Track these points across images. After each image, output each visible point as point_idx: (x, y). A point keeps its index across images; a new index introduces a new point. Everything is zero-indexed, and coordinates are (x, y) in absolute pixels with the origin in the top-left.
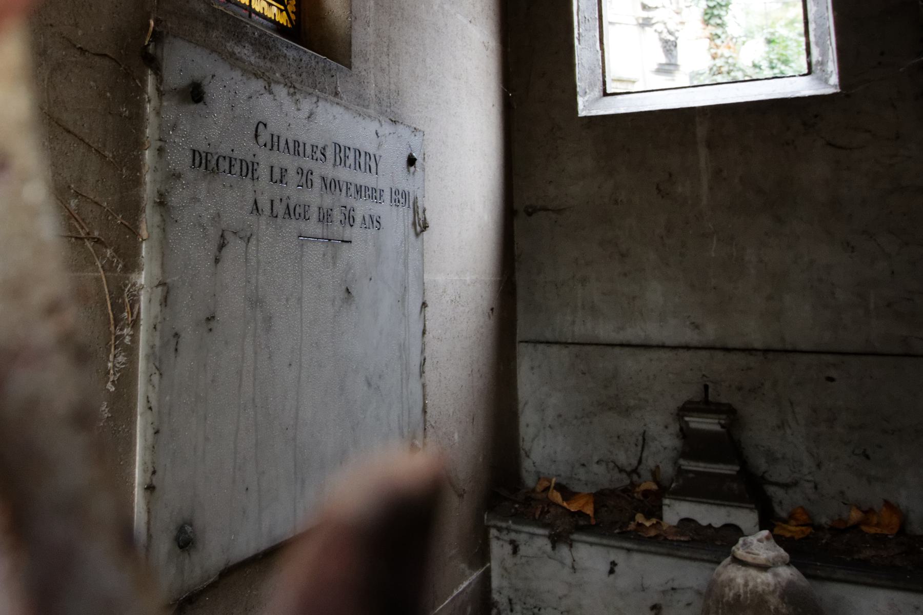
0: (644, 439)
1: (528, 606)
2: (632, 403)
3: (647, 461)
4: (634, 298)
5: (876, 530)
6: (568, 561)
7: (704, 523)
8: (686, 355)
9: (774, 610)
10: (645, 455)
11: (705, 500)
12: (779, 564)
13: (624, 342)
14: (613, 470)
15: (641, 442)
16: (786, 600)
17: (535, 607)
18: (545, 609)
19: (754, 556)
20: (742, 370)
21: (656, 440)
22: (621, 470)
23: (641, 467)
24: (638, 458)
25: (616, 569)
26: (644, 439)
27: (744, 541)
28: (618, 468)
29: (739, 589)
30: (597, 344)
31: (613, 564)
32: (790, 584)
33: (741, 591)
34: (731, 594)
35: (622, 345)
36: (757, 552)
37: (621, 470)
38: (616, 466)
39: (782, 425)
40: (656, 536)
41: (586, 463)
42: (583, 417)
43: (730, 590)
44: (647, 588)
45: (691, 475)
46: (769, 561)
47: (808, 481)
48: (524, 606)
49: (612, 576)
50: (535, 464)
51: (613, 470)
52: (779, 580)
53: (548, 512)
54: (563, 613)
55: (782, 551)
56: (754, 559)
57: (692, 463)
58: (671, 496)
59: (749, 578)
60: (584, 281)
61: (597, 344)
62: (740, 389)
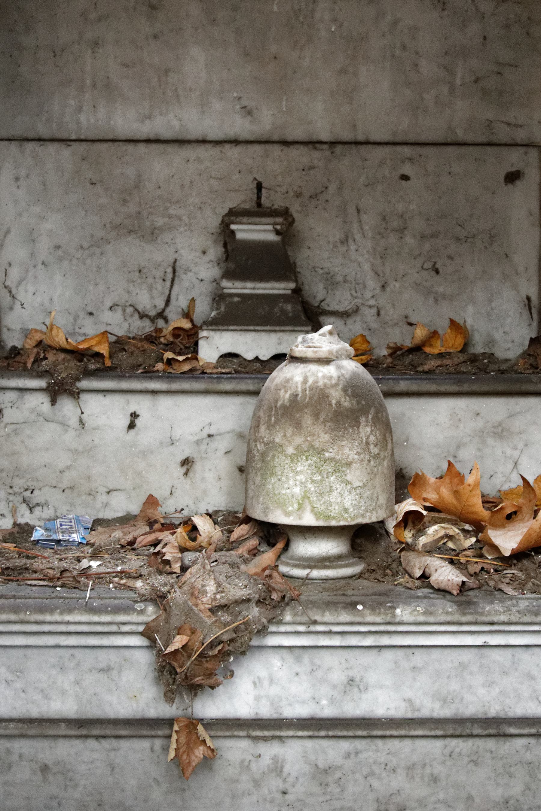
0: (174, 271)
1: (16, 490)
2: (160, 222)
3: (177, 300)
4: (167, 71)
5: (440, 350)
6: (74, 422)
7: (249, 356)
8: (233, 152)
9: (336, 404)
10: (174, 292)
11: (252, 328)
12: (343, 357)
13: (152, 137)
14: (132, 316)
15: (170, 276)
16: (349, 392)
17: (26, 490)
18: (40, 489)
19: (316, 349)
20: (303, 170)
21: (190, 271)
22: (142, 316)
23: (168, 309)
24: (166, 298)
25: (137, 422)
26: (174, 271)
27: (303, 338)
28: (139, 313)
29: (297, 387)
30: (113, 141)
31: (134, 415)
32: (355, 376)
33: (300, 389)
34: (287, 396)
35: (148, 141)
36: (318, 345)
37: (142, 316)
38: (136, 310)
39: (345, 241)
40: (191, 371)
41: (94, 312)
42: (92, 246)
43: (286, 391)
44: (177, 441)
45: (236, 299)
46: (333, 354)
47: (370, 307)
48: (11, 491)
49: (132, 432)
50: (24, 306)
51: (132, 316)
52: (343, 372)
53: (45, 358)
54: (65, 491)
55: (347, 345)
56: (316, 352)
57: (238, 284)
58: (210, 328)
59: (308, 374)
60: (95, 44)
61: (113, 141)
62: (298, 195)
